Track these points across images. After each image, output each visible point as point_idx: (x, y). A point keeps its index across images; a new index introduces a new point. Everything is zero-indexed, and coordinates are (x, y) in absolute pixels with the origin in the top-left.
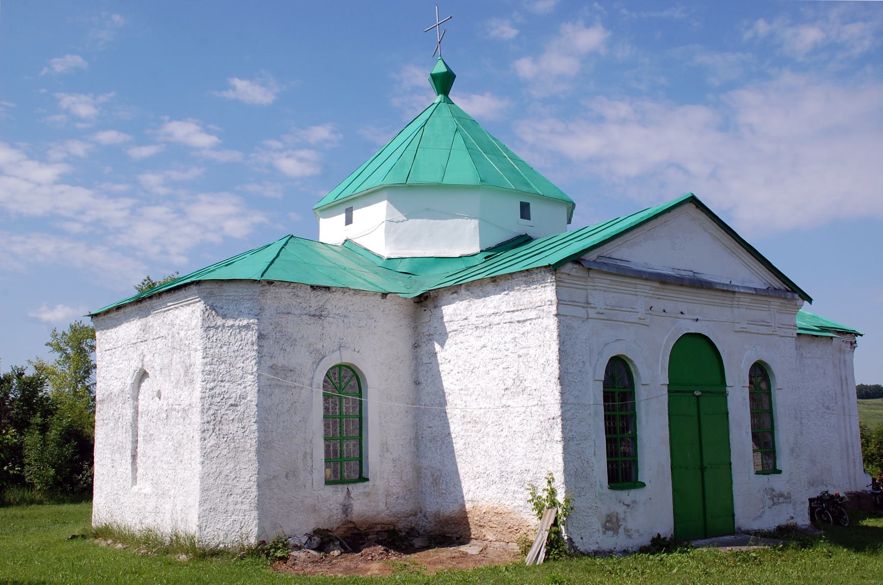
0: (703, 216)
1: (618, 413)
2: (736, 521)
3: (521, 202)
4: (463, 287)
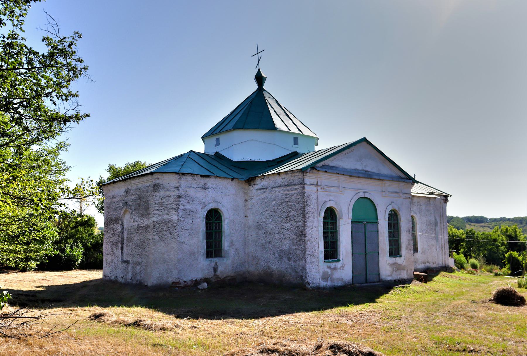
0: (370, 147)
1: (330, 231)
2: (380, 276)
3: (294, 137)
4: (266, 176)
